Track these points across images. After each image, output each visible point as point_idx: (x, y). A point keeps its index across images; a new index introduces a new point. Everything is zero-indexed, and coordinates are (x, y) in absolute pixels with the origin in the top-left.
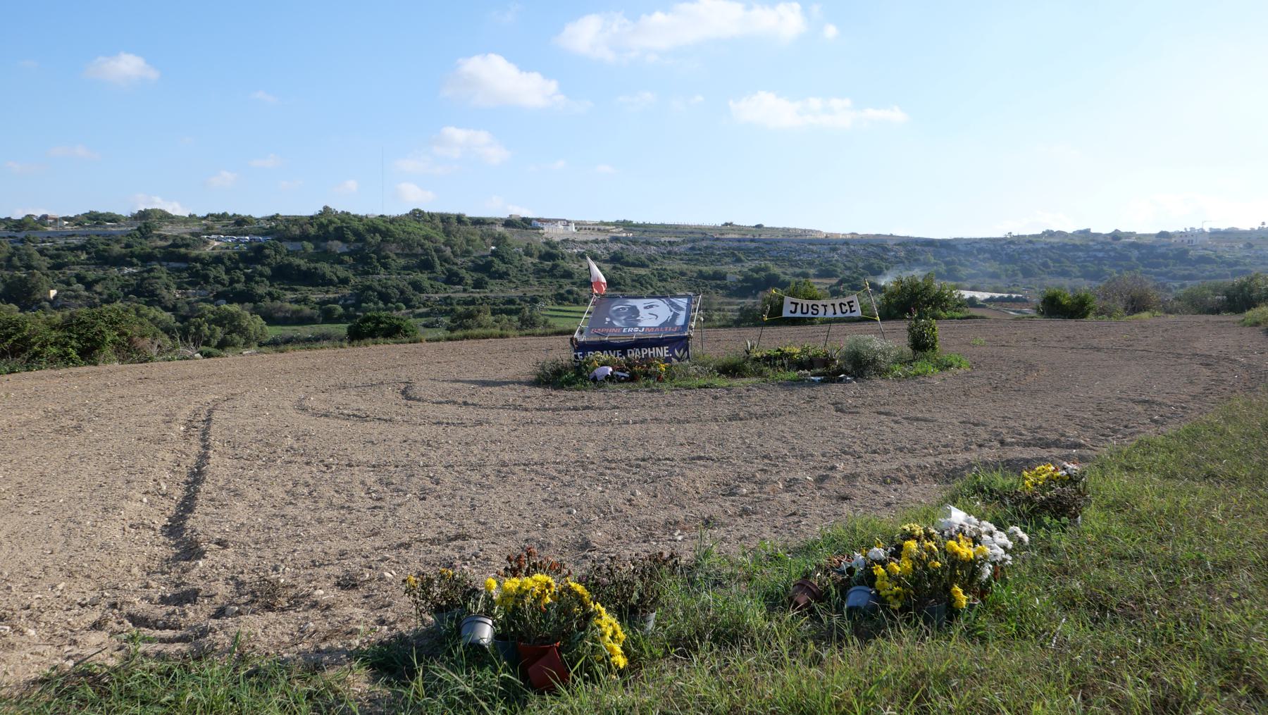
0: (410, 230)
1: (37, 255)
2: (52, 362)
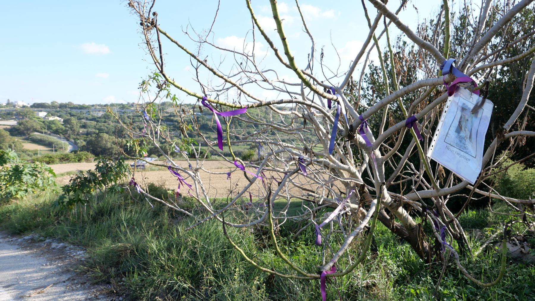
0: (251, 112)
1: (127, 118)
2: (73, 162)
